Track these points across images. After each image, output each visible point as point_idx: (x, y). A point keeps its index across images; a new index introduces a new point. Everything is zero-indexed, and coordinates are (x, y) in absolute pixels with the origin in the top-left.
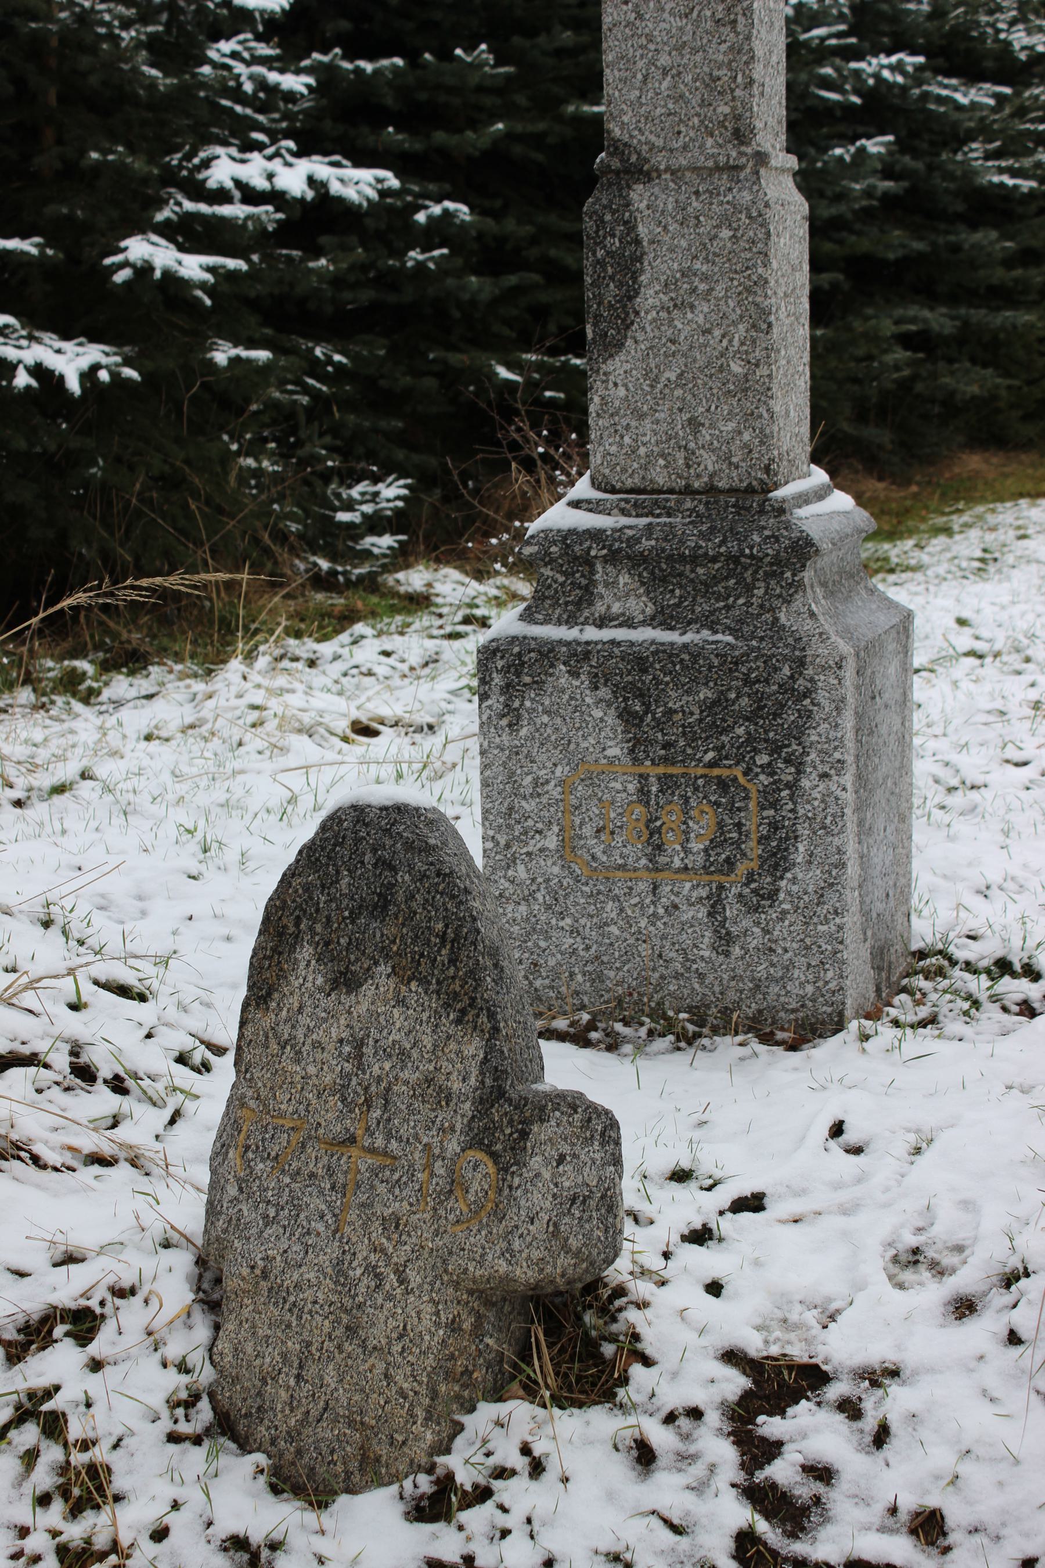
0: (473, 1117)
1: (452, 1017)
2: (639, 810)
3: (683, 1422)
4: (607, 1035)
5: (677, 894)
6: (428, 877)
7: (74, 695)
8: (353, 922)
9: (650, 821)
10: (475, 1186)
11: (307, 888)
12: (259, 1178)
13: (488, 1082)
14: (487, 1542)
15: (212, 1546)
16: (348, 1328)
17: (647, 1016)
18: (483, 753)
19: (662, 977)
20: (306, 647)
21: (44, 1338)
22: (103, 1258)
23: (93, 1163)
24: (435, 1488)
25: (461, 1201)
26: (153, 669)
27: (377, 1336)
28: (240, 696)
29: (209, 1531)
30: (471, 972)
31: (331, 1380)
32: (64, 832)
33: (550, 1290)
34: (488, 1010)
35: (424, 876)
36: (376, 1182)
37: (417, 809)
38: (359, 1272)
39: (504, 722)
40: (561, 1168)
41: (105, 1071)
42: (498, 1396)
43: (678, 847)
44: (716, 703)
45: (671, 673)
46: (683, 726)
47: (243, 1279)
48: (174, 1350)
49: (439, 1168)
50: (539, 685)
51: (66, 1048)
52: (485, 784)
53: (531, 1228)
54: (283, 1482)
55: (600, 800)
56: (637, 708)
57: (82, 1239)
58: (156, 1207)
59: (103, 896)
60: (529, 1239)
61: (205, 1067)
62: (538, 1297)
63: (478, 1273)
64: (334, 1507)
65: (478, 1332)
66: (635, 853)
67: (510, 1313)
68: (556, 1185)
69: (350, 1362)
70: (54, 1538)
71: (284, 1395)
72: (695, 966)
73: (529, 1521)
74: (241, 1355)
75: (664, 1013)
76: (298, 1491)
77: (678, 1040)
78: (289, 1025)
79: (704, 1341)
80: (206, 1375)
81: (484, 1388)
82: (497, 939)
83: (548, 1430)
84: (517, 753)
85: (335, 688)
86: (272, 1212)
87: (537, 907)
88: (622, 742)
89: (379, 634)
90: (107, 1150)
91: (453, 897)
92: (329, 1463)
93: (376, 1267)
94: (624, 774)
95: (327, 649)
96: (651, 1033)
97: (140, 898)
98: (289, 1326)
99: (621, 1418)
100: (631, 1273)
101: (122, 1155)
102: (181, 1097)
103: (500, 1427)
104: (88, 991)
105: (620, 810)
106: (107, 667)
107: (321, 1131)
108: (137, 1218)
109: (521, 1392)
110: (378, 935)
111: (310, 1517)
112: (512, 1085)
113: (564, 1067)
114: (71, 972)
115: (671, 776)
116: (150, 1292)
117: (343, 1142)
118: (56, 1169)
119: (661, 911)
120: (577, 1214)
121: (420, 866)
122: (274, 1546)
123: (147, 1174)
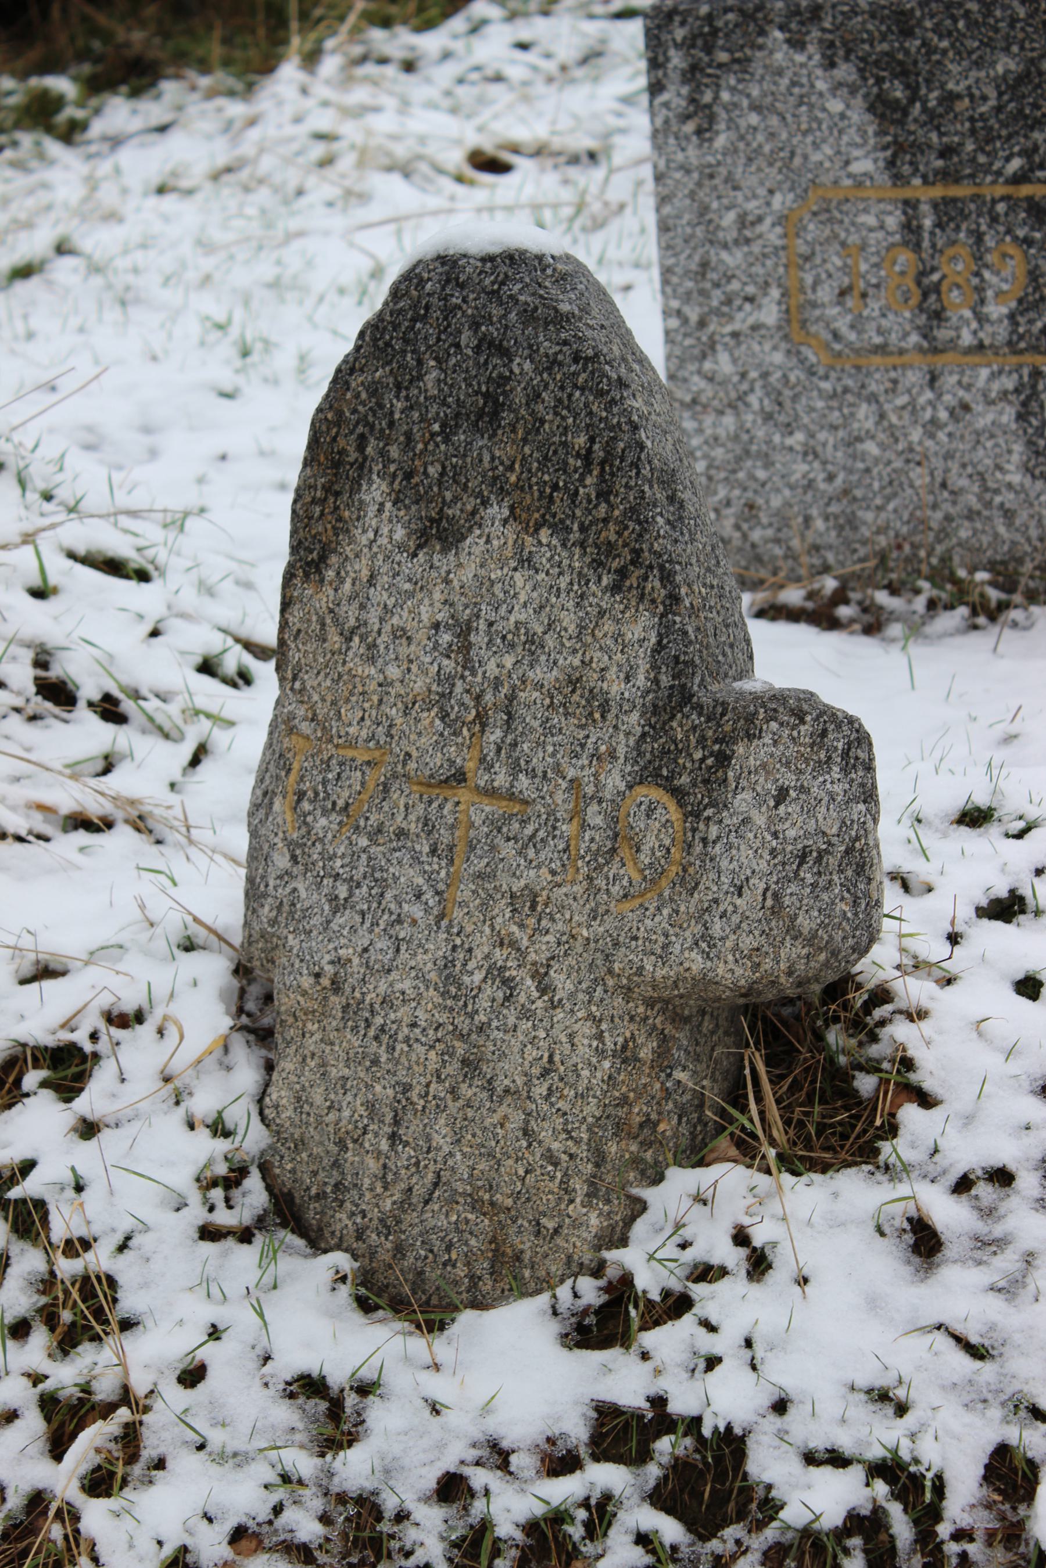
0: (644, 735)
1: (605, 581)
2: (905, 258)
3: (984, 1190)
4: (865, 610)
5: (968, 388)
6: (561, 364)
7: (50, 130)
8: (447, 440)
9: (922, 274)
10: (650, 841)
11: (374, 390)
12: (321, 840)
13: (665, 680)
14: (686, 1375)
15: (272, 1391)
16: (465, 1062)
17: (927, 578)
18: (659, 178)
19: (948, 518)
20: (401, 41)
21: (10, 1091)
22: (92, 970)
23: (76, 828)
24: (605, 1298)
25: (630, 864)
26: (169, 88)
27: (509, 1072)
28: (298, 120)
29: (266, 1369)
30: (633, 511)
31: (442, 1139)
32: (30, 336)
33: (770, 995)
34: (662, 568)
35: (554, 363)
36: (499, 841)
37: (540, 258)
38: (478, 977)
39: (689, 127)
40: (782, 808)
41: (89, 690)
42: (697, 1156)
43: (968, 313)
44: (1022, 78)
45: (950, 34)
46: (972, 119)
47: (304, 993)
48: (204, 1102)
49: (595, 816)
50: (742, 64)
51: (28, 656)
52: (664, 227)
53: (738, 902)
54: (375, 1294)
55: (843, 244)
56: (898, 94)
57: (61, 942)
58: (172, 891)
59: (90, 429)
60: (735, 919)
61: (244, 678)
62: (756, 1006)
63: (660, 973)
64: (454, 1330)
65: (663, 1063)
66: (900, 326)
67: (713, 1033)
68: (775, 834)
69: (470, 1113)
70: (35, 1385)
71: (372, 1165)
72: (998, 499)
73: (749, 1343)
74: (306, 1107)
75: (952, 573)
76: (399, 1306)
77: (974, 613)
78: (356, 604)
79: (1014, 1067)
80: (254, 1138)
81: (676, 1146)
82: (672, 458)
83: (774, 1207)
84: (711, 176)
85: (446, 103)
86: (342, 892)
87: (750, 417)
88: (875, 149)
89: (512, 16)
90: (95, 807)
91: (601, 393)
92: (445, 1264)
93: (503, 969)
94: (880, 201)
95: (430, 42)
96: (932, 605)
97: (147, 430)
98: (375, 1062)
99: (887, 1186)
100: (898, 967)
101: (119, 815)
102: (205, 724)
103: (698, 1205)
104: (59, 569)
105: (875, 259)
106: (98, 85)
107: (412, 765)
108: (142, 907)
109: (733, 1152)
110: (487, 458)
111: (417, 1345)
112: (702, 684)
113: (785, 658)
114: (28, 538)
115: (954, 200)
116: (166, 1018)
117: (446, 781)
118: (20, 839)
119: (943, 415)
120: (809, 878)
121: (547, 347)
122: (364, 1389)
123: (159, 842)
